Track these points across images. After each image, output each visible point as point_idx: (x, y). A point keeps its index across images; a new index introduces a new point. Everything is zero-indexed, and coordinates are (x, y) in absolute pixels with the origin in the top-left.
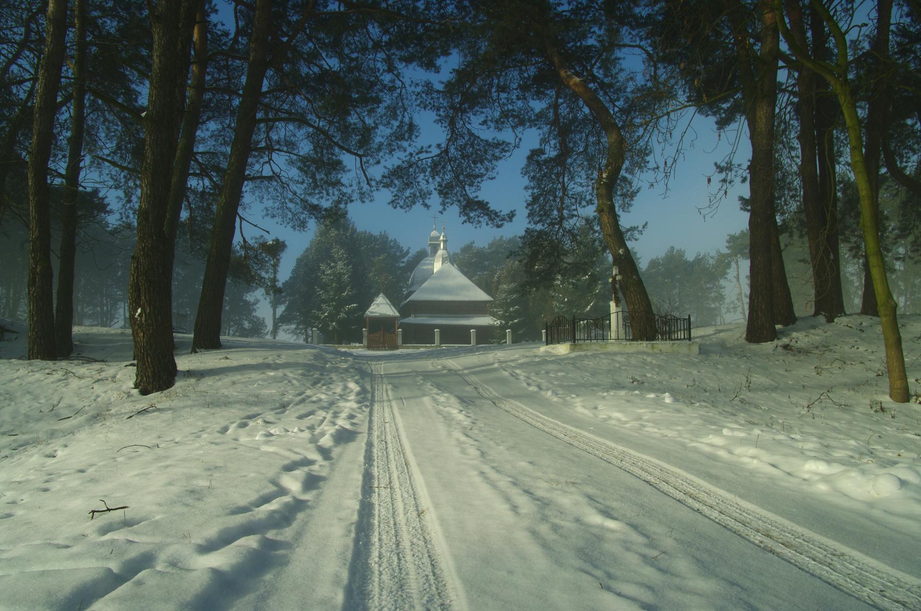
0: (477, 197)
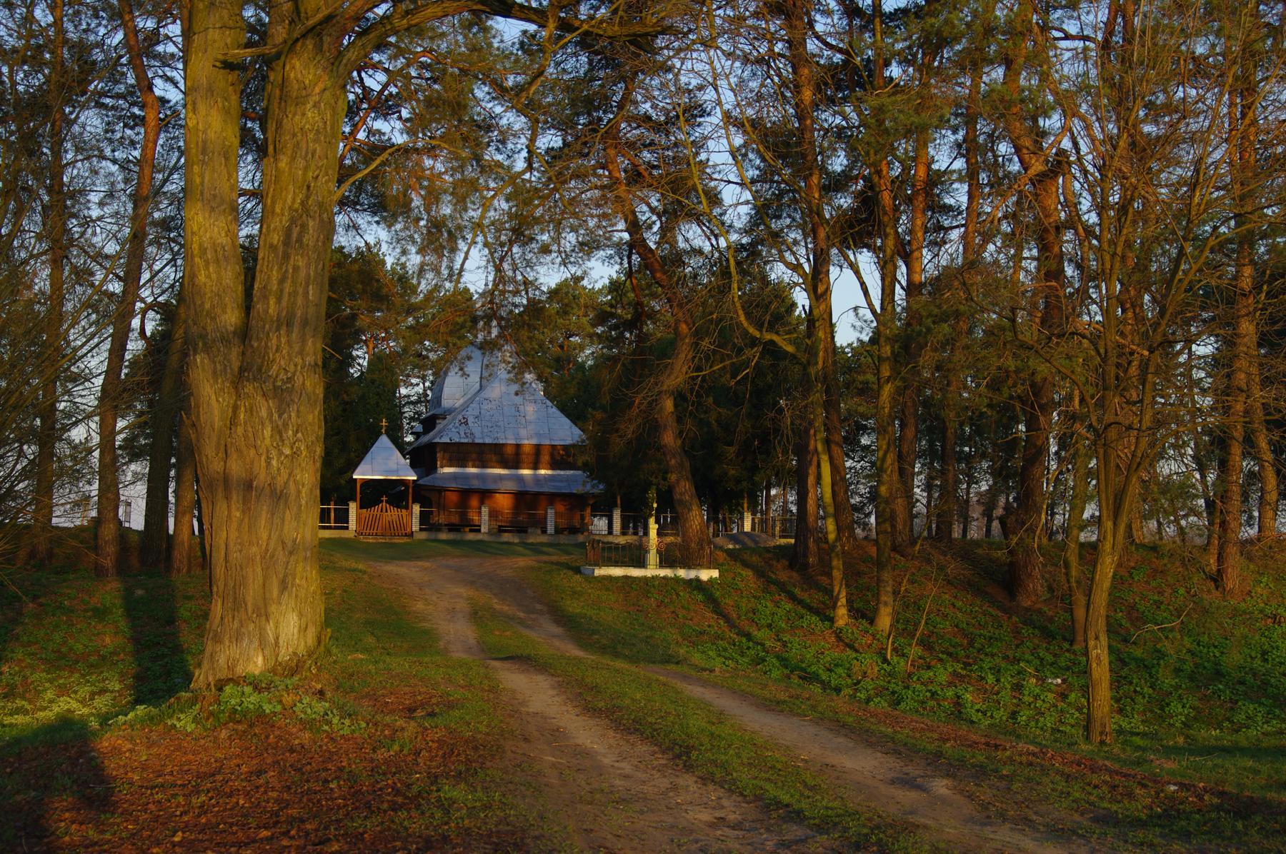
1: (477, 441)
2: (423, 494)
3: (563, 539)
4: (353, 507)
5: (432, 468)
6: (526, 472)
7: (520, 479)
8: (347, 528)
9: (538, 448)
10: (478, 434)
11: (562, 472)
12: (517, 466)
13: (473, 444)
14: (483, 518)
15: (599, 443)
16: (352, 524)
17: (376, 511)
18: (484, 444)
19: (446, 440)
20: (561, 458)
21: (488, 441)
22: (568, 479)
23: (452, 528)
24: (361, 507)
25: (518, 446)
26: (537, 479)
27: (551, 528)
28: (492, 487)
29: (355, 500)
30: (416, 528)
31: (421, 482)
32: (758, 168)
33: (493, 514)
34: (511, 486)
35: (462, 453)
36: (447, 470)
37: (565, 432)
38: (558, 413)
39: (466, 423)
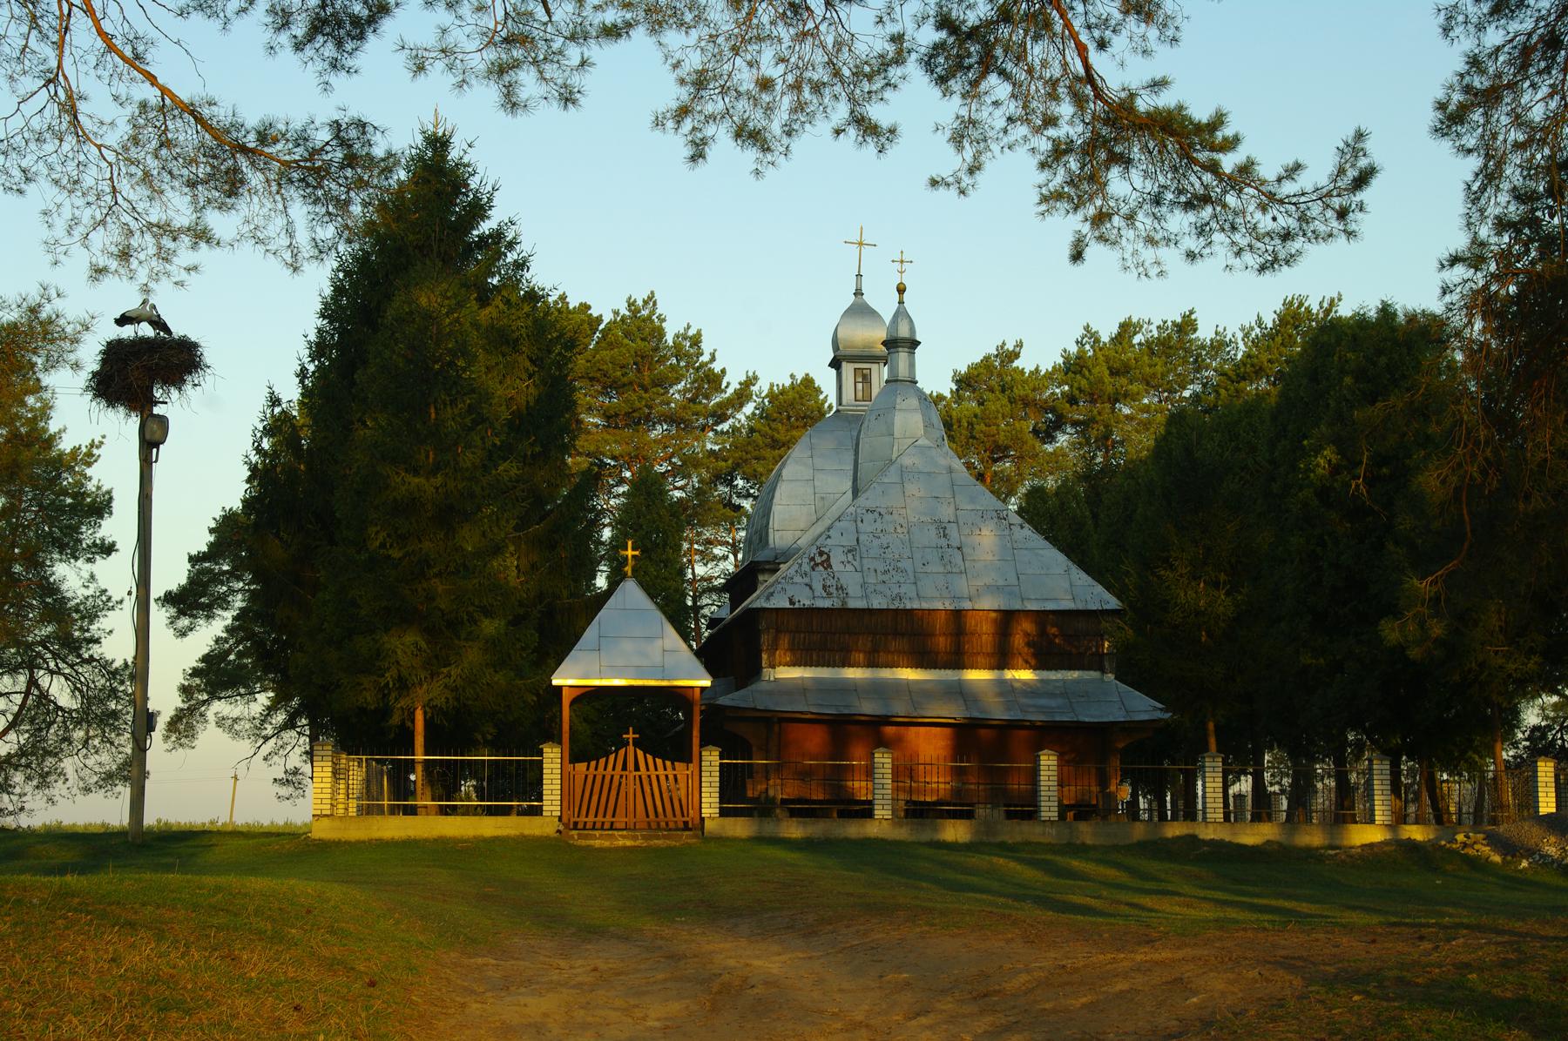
0: (1158, 85)
1: (852, 604)
2: (739, 733)
3: (1087, 832)
4: (552, 759)
5: (752, 672)
6: (977, 676)
7: (960, 692)
8: (537, 811)
9: (1007, 618)
10: (854, 589)
11: (1075, 674)
12: (958, 661)
13: (844, 612)
14: (879, 779)
15: (1144, 608)
16: (552, 799)
17: (608, 767)
18: (870, 612)
19: (781, 602)
20: (1056, 638)
21: (877, 603)
22: (1065, 691)
23: (801, 809)
24: (575, 757)
25: (958, 615)
26: (1007, 690)
27: (1049, 810)
28: (900, 709)
29: (554, 737)
30: (710, 804)
31: (724, 700)
32: (234, 575)
33: (905, 772)
34: (952, 711)
35: (831, 633)
36: (789, 674)
37: (1063, 584)
38: (1038, 541)
39: (827, 564)
